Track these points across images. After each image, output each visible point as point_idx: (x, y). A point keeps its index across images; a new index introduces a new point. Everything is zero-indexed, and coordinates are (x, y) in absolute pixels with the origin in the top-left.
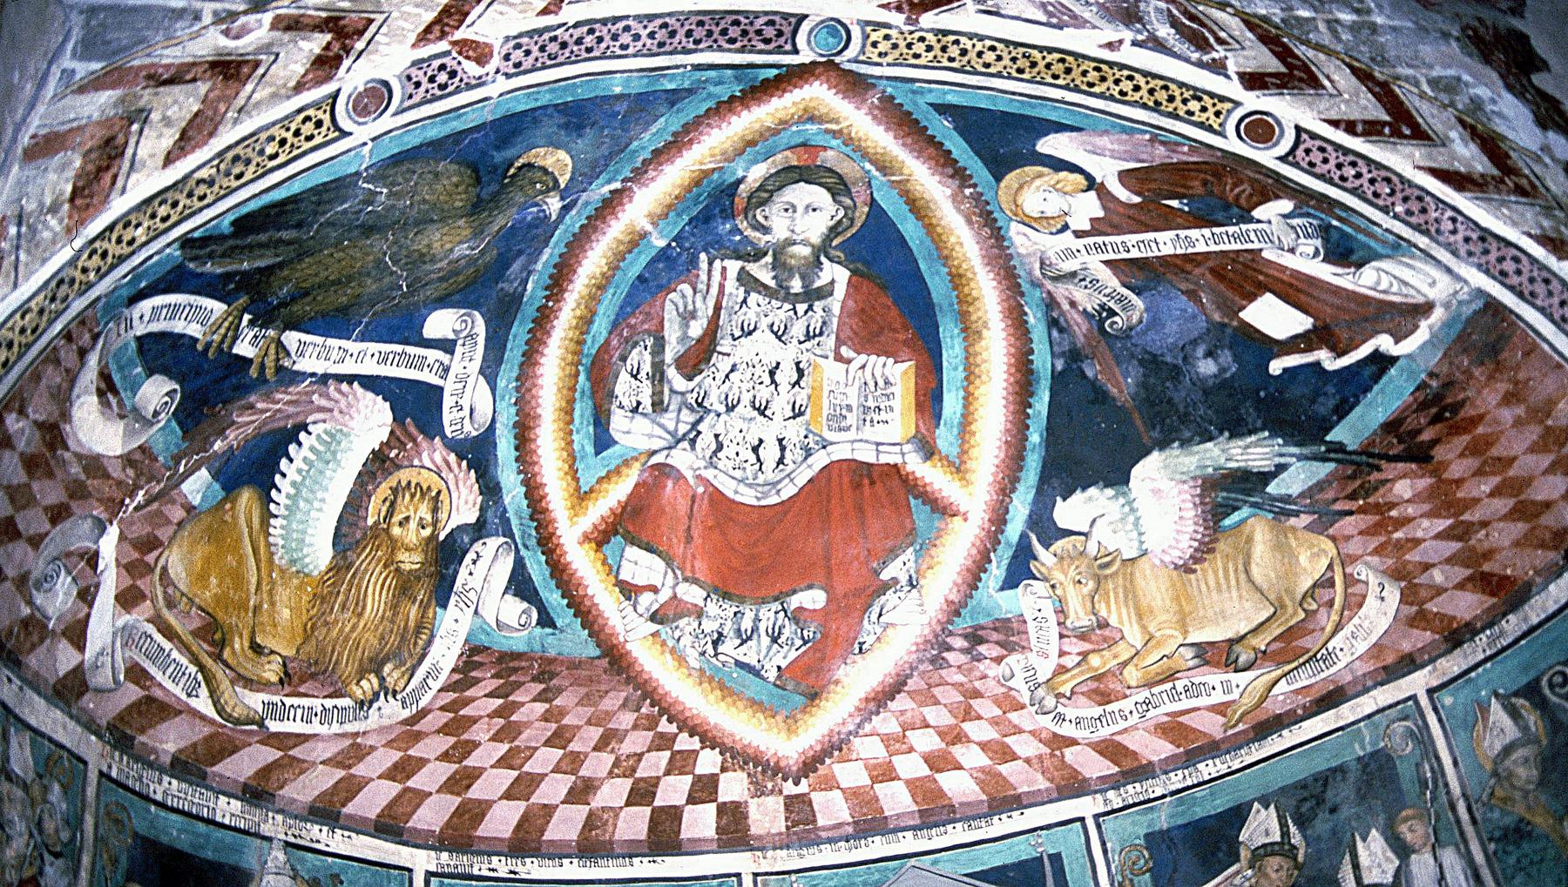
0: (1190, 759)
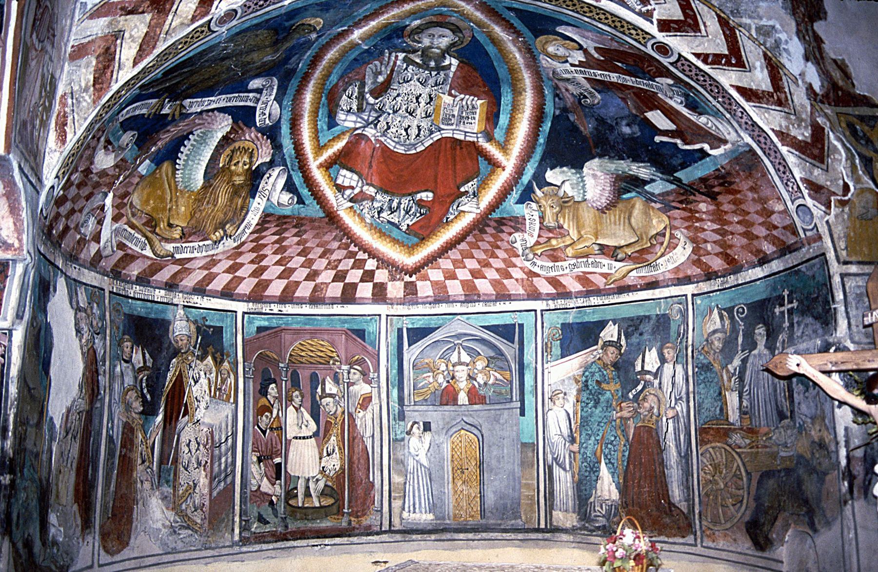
0: (588, 294)
